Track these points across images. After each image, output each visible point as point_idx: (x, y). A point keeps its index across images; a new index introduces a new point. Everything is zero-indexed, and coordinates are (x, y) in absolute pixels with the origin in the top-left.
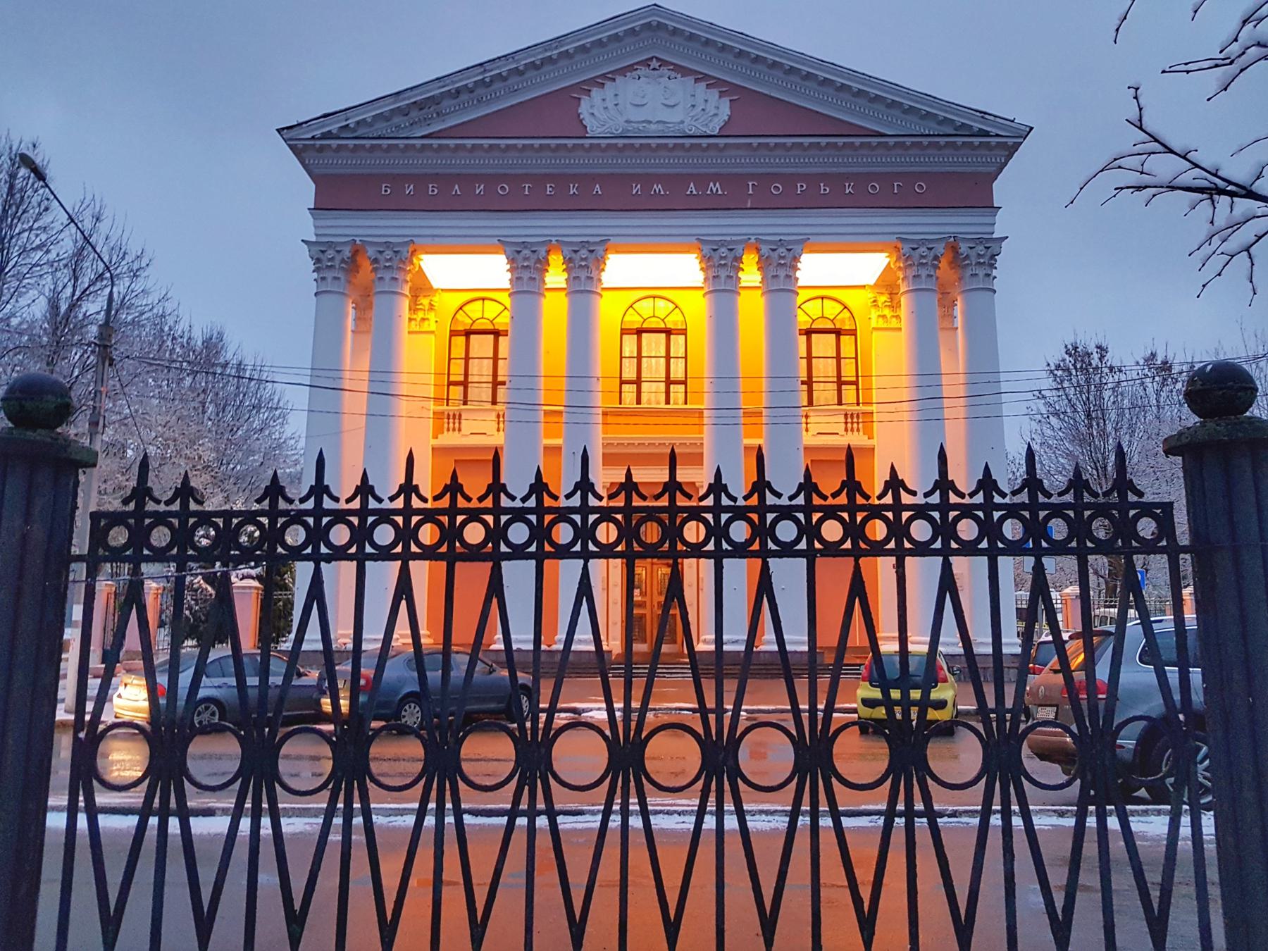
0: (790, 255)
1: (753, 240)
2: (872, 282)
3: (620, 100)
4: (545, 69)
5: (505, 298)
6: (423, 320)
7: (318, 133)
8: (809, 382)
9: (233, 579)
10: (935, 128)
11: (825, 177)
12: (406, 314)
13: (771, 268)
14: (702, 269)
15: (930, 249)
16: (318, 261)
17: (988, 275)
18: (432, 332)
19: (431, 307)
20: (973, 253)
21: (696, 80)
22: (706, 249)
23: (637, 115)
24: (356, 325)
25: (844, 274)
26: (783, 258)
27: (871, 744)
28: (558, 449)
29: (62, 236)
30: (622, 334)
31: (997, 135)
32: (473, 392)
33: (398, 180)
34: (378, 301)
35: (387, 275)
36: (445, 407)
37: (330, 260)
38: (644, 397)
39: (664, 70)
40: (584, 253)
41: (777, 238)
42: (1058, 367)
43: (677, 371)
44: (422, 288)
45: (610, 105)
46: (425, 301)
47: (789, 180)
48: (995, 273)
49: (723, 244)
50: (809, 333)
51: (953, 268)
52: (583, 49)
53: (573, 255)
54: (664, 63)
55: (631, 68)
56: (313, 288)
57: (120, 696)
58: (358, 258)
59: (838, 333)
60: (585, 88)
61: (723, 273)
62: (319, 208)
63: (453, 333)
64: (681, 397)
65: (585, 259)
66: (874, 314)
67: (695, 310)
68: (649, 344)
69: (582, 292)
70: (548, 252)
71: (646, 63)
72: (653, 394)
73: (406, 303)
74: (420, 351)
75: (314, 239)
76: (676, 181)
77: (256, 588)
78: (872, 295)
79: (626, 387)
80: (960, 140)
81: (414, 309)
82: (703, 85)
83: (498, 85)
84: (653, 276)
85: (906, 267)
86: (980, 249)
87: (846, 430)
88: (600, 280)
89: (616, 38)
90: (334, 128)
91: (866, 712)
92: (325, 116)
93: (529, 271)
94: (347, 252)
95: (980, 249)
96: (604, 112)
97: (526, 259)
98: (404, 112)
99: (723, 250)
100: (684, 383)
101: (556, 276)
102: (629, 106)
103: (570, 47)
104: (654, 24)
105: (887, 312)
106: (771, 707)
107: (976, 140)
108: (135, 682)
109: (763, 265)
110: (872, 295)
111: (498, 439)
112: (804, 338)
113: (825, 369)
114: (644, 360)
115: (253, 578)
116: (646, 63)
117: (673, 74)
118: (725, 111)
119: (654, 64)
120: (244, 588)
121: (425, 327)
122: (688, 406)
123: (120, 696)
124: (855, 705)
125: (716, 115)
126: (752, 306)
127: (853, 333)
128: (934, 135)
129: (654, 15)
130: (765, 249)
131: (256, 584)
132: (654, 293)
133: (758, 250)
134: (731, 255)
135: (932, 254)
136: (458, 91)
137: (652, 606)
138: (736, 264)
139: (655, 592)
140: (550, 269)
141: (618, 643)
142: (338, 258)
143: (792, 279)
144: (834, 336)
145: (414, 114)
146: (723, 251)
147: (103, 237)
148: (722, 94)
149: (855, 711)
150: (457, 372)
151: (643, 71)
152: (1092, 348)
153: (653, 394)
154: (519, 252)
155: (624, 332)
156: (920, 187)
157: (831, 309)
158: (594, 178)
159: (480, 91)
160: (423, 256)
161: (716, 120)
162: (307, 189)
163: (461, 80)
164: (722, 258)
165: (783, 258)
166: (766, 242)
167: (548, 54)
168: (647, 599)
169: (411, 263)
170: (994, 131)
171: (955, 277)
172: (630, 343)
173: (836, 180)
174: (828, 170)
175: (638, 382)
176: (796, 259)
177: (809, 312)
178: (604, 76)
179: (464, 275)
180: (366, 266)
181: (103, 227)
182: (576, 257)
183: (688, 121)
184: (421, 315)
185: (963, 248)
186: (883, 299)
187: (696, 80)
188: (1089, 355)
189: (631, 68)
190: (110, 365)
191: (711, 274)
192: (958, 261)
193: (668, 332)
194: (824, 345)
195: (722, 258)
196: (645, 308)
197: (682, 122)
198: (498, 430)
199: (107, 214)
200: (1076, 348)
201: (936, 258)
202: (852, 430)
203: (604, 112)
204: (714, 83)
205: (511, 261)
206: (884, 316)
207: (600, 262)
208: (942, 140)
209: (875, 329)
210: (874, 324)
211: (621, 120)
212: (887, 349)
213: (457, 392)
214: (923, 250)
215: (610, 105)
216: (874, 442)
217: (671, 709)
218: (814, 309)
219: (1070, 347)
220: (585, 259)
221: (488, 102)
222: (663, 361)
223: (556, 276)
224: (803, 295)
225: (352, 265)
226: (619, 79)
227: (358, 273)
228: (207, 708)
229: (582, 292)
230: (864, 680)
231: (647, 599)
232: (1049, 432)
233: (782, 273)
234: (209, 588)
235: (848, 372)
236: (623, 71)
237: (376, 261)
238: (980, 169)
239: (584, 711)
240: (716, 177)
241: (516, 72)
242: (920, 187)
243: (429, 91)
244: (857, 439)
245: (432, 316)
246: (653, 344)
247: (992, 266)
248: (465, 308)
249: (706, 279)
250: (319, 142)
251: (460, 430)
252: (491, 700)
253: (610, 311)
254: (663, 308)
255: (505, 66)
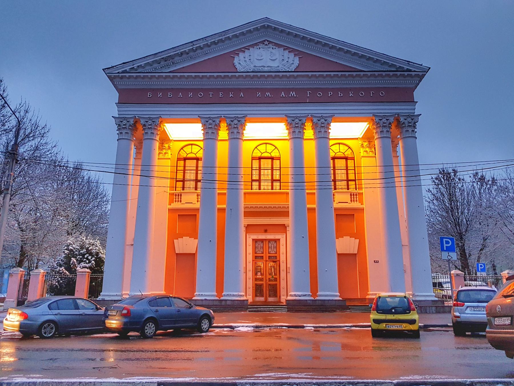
0: (326, 122)
1: (310, 116)
2: (361, 137)
3: (251, 58)
4: (220, 44)
5: (201, 144)
6: (165, 153)
7: (120, 71)
8: (335, 181)
9: (78, 268)
10: (386, 68)
11: (341, 90)
12: (157, 151)
13: (318, 128)
14: (287, 129)
15: (387, 120)
16: (119, 125)
17: (413, 131)
18: (169, 159)
19: (169, 148)
20: (406, 122)
21: (284, 49)
22: (289, 120)
23: (258, 64)
24: (136, 156)
25: (349, 132)
26: (323, 123)
27: (381, 342)
28: (224, 209)
29: (11, 118)
30: (252, 160)
31: (415, 71)
32: (187, 184)
33: (155, 91)
34: (145, 143)
35: (149, 132)
36: (175, 191)
37: (124, 125)
38: (262, 187)
39: (271, 45)
40: (236, 122)
41: (321, 115)
42: (436, 179)
43: (277, 177)
44: (165, 139)
45: (247, 59)
46: (166, 146)
47: (325, 91)
48: (416, 130)
49: (297, 118)
50: (334, 158)
51: (396, 127)
52: (236, 36)
53: (231, 122)
54: (270, 42)
55: (256, 44)
56: (117, 137)
57: (6, 320)
58: (137, 125)
59: (346, 158)
60: (236, 53)
61: (297, 130)
62: (120, 103)
63: (179, 159)
64: (278, 187)
65: (236, 124)
66: (362, 150)
67: (285, 149)
68: (264, 164)
69: (234, 138)
70: (220, 121)
71: (263, 42)
72: (266, 186)
73: (157, 144)
74: (163, 164)
75: (117, 116)
76: (275, 91)
77: (88, 272)
78: (360, 142)
79: (254, 183)
80: (399, 73)
81: (161, 148)
82: (287, 51)
83: (199, 51)
84: (266, 134)
85: (377, 128)
86: (409, 120)
87: (351, 201)
88: (243, 134)
89: (250, 31)
90: (127, 68)
91: (375, 326)
92: (124, 63)
93: (211, 129)
94: (132, 122)
95: (409, 120)
96: (244, 62)
97: (210, 124)
98: (158, 62)
99: (297, 120)
100: (279, 180)
101: (223, 134)
102: (255, 60)
103: (230, 35)
104: (266, 26)
105: (367, 149)
106: (326, 325)
107: (406, 73)
108: (14, 312)
109: (314, 127)
110: (360, 142)
111: (198, 205)
112: (332, 161)
113: (341, 175)
114: (262, 171)
115: (87, 268)
116: (263, 42)
117: (274, 47)
118: (297, 61)
119: (266, 43)
120: (83, 272)
121: (166, 156)
122: (281, 191)
123: (6, 320)
124: (370, 324)
125: (293, 63)
126: (310, 147)
127: (353, 159)
128: (387, 71)
129: (266, 22)
130: (315, 120)
131: (88, 270)
132: (266, 142)
133: (312, 120)
134: (300, 123)
135: (388, 122)
136: (182, 54)
137: (266, 280)
138: (302, 127)
139: (267, 274)
140: (221, 129)
141: (251, 297)
142: (128, 124)
143: (327, 133)
144: (344, 160)
145: (163, 63)
146: (297, 121)
147: (29, 119)
148: (295, 55)
149: (370, 326)
150: (180, 176)
151: (261, 46)
152: (450, 170)
153: (266, 186)
154: (207, 121)
155: (253, 158)
156: (382, 94)
157: (343, 148)
158: (240, 90)
159: (191, 54)
160: (165, 124)
161: (293, 66)
162: (115, 96)
163: (183, 49)
164: (296, 124)
165: (323, 123)
166: (315, 117)
167: (221, 38)
168: (264, 277)
169: (161, 127)
170: (413, 69)
171: (398, 132)
172: (256, 164)
173: (345, 90)
174: (342, 86)
175: (259, 181)
176: (329, 124)
177: (335, 150)
178: (244, 48)
179: (184, 132)
180: (140, 128)
181: (29, 115)
182: (232, 123)
183: (280, 67)
184: (164, 151)
185: (402, 119)
186: (365, 144)
187: (284, 49)
188: (449, 174)
189: (256, 44)
190: (16, 163)
191: (292, 130)
192: (399, 125)
193: (272, 159)
194: (340, 164)
195: (296, 124)
196: (262, 148)
197: (278, 66)
198: (198, 201)
199: (31, 110)
200: (444, 171)
201: (390, 124)
202: (354, 201)
203: (244, 62)
204: (291, 50)
205: (204, 125)
206: (366, 151)
207: (243, 126)
208: (391, 73)
209: (362, 157)
210: (362, 155)
211: (252, 66)
212: (369, 164)
213: (180, 184)
214: (384, 120)
215: (247, 59)
216: (364, 206)
217: (278, 326)
218: (335, 148)
219: (441, 170)
220: (236, 124)
221: (195, 58)
222: (270, 171)
223: (223, 134)
224: (331, 142)
225: (134, 127)
226: (251, 49)
227: (137, 132)
228: (49, 325)
229: (234, 138)
230: (373, 310)
231: (264, 277)
232: (433, 207)
233: (323, 130)
234: (67, 273)
235: (351, 177)
236: (253, 46)
237: (144, 125)
238: (409, 86)
239: (235, 327)
240: (293, 90)
241: (208, 46)
242: (382, 94)
243: (169, 53)
244: (356, 205)
245: (169, 152)
246: (266, 164)
247: (415, 127)
248: (184, 149)
249: (289, 133)
250: (120, 75)
251: (181, 201)
252: (191, 321)
253: (247, 149)
254: (270, 148)
255: (202, 43)
